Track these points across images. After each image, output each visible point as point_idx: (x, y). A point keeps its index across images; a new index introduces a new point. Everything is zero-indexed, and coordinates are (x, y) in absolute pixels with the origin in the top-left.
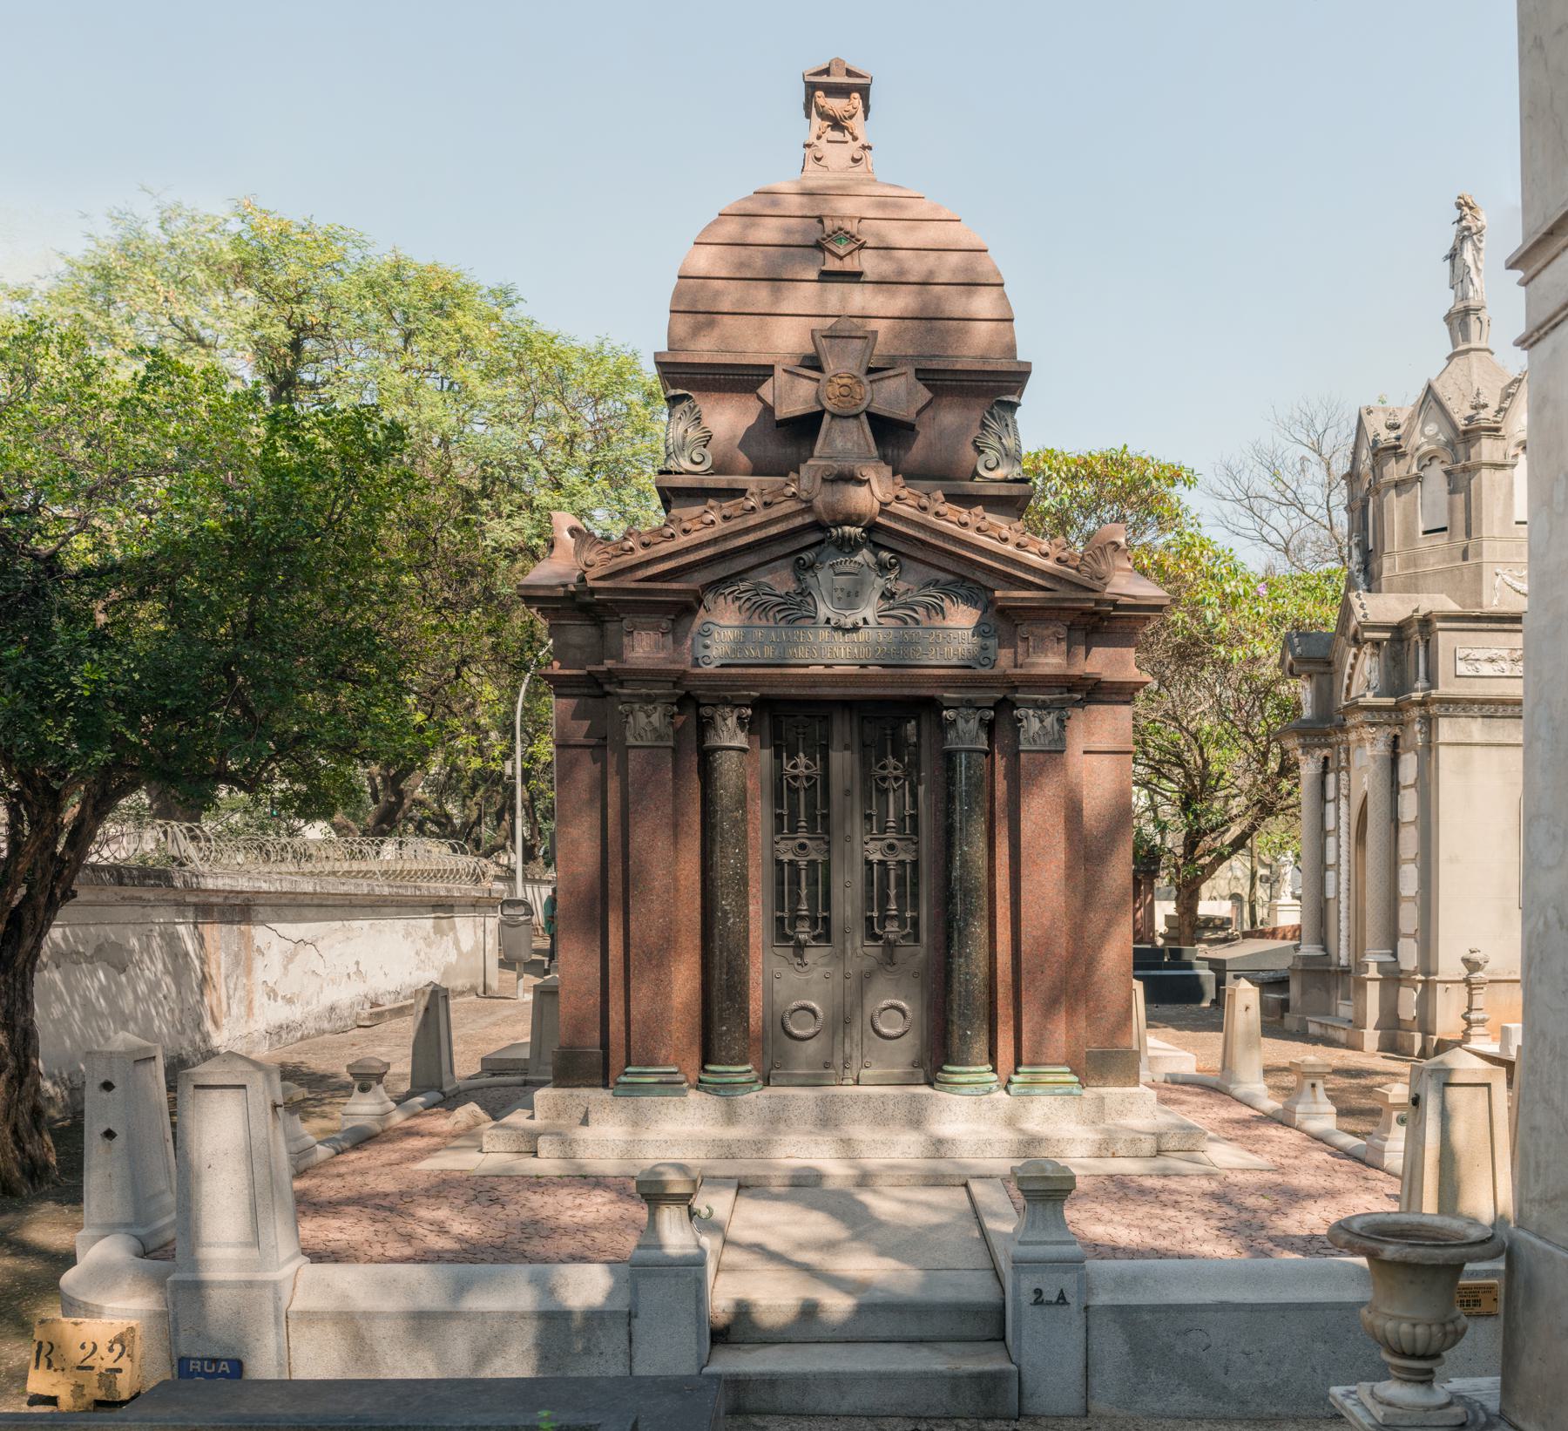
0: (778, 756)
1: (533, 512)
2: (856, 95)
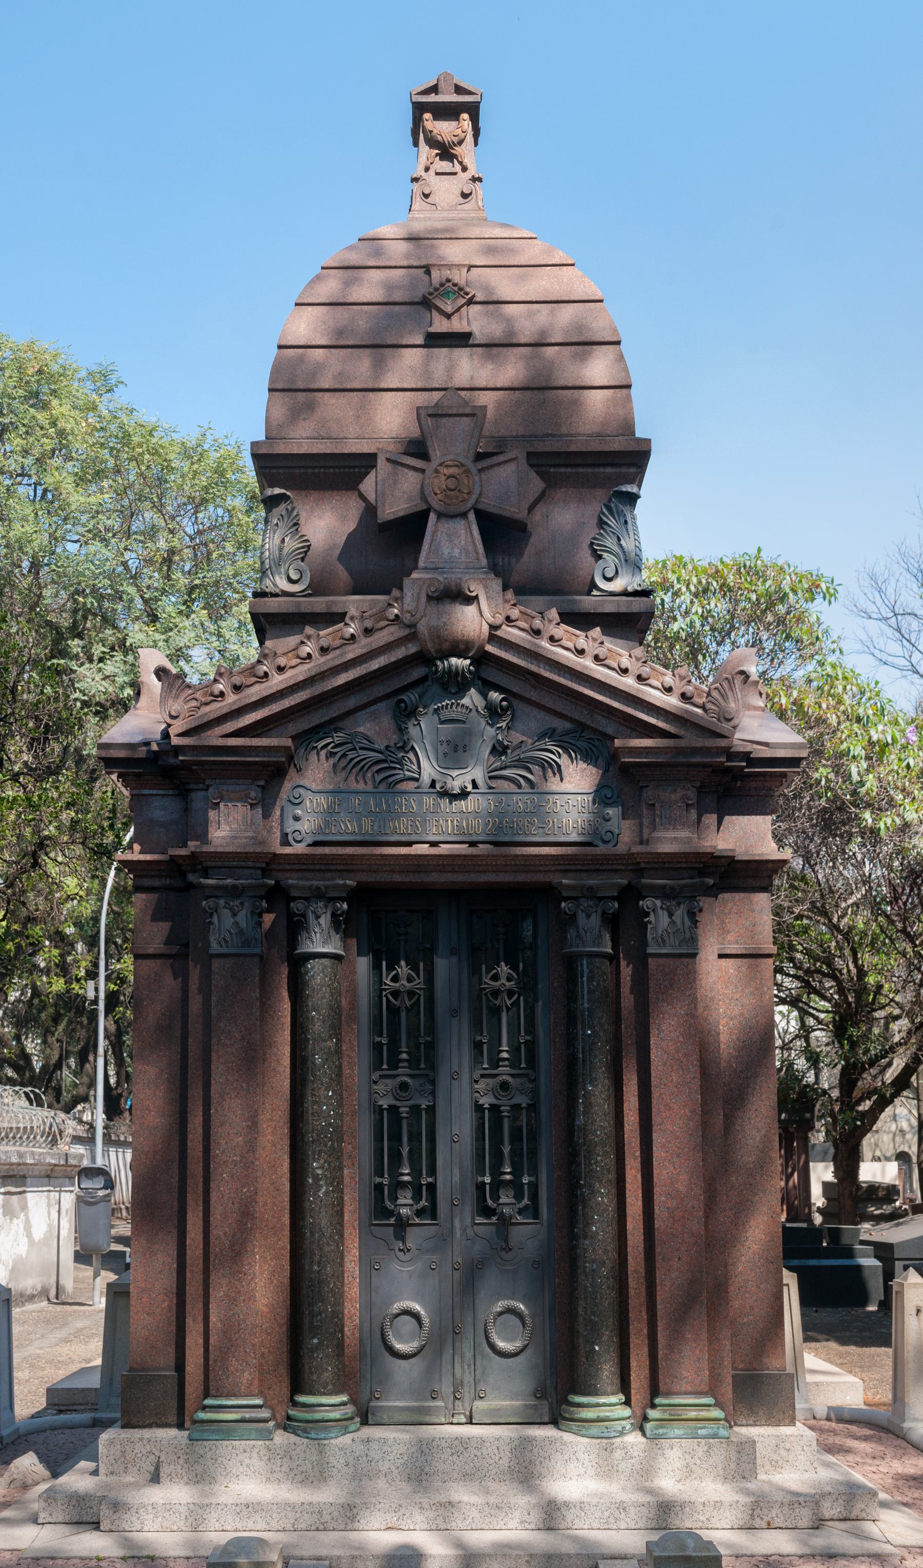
0: (376, 966)
1: (126, 654)
2: (465, 116)
